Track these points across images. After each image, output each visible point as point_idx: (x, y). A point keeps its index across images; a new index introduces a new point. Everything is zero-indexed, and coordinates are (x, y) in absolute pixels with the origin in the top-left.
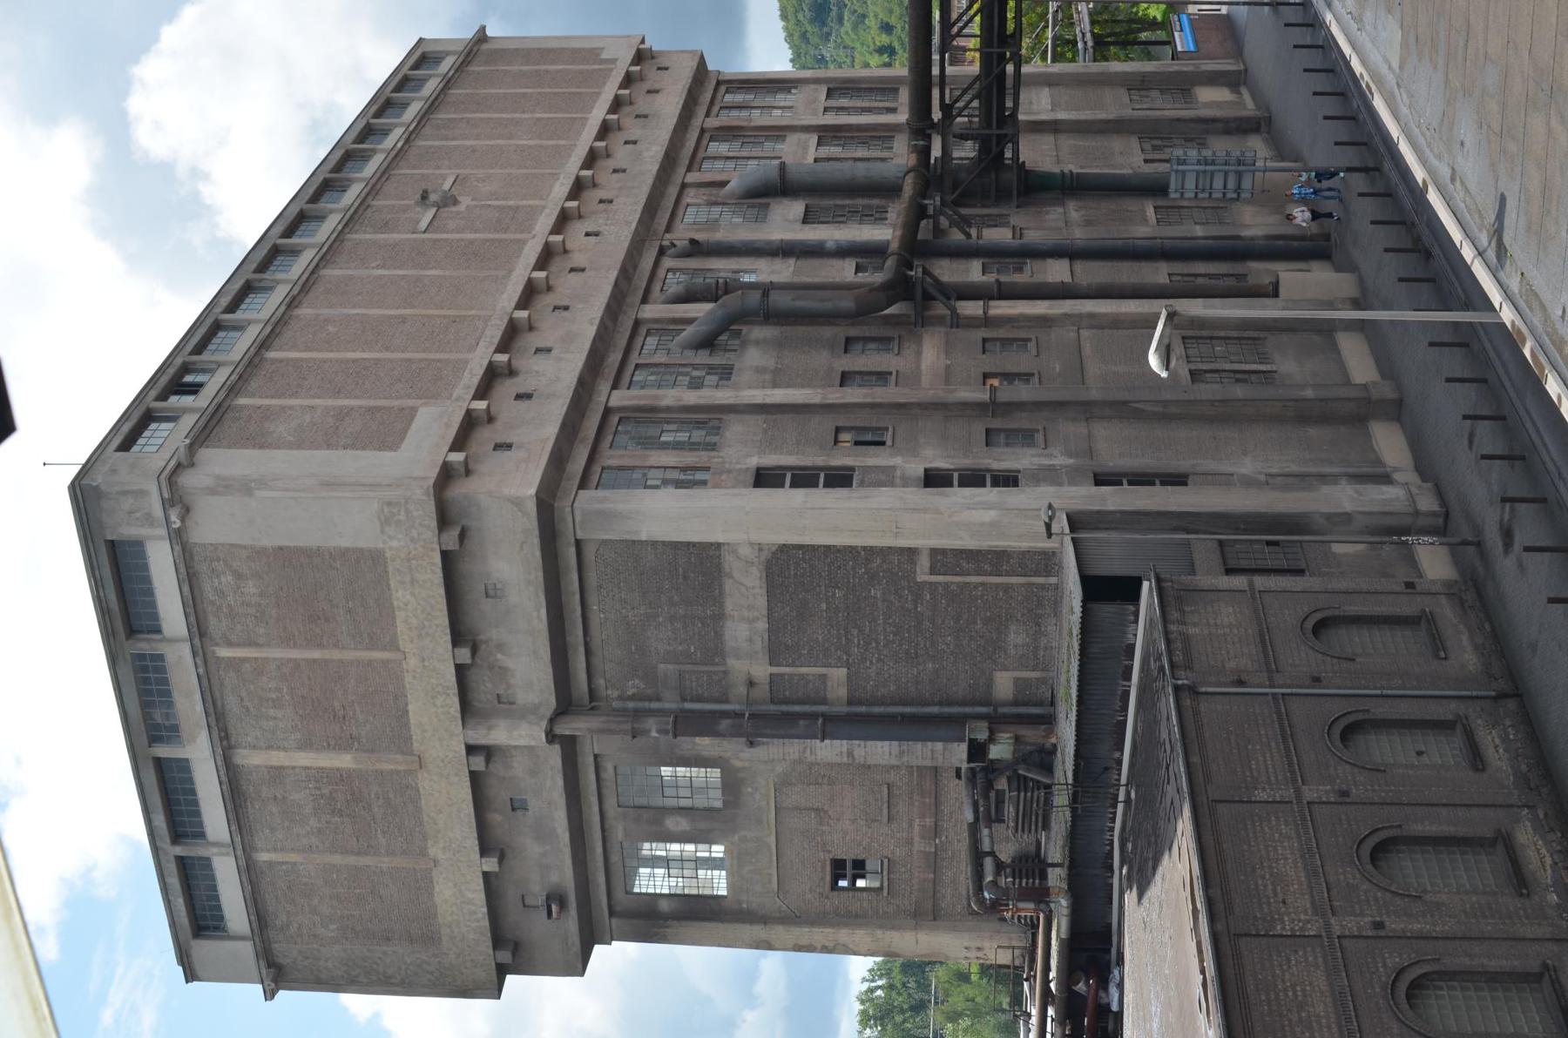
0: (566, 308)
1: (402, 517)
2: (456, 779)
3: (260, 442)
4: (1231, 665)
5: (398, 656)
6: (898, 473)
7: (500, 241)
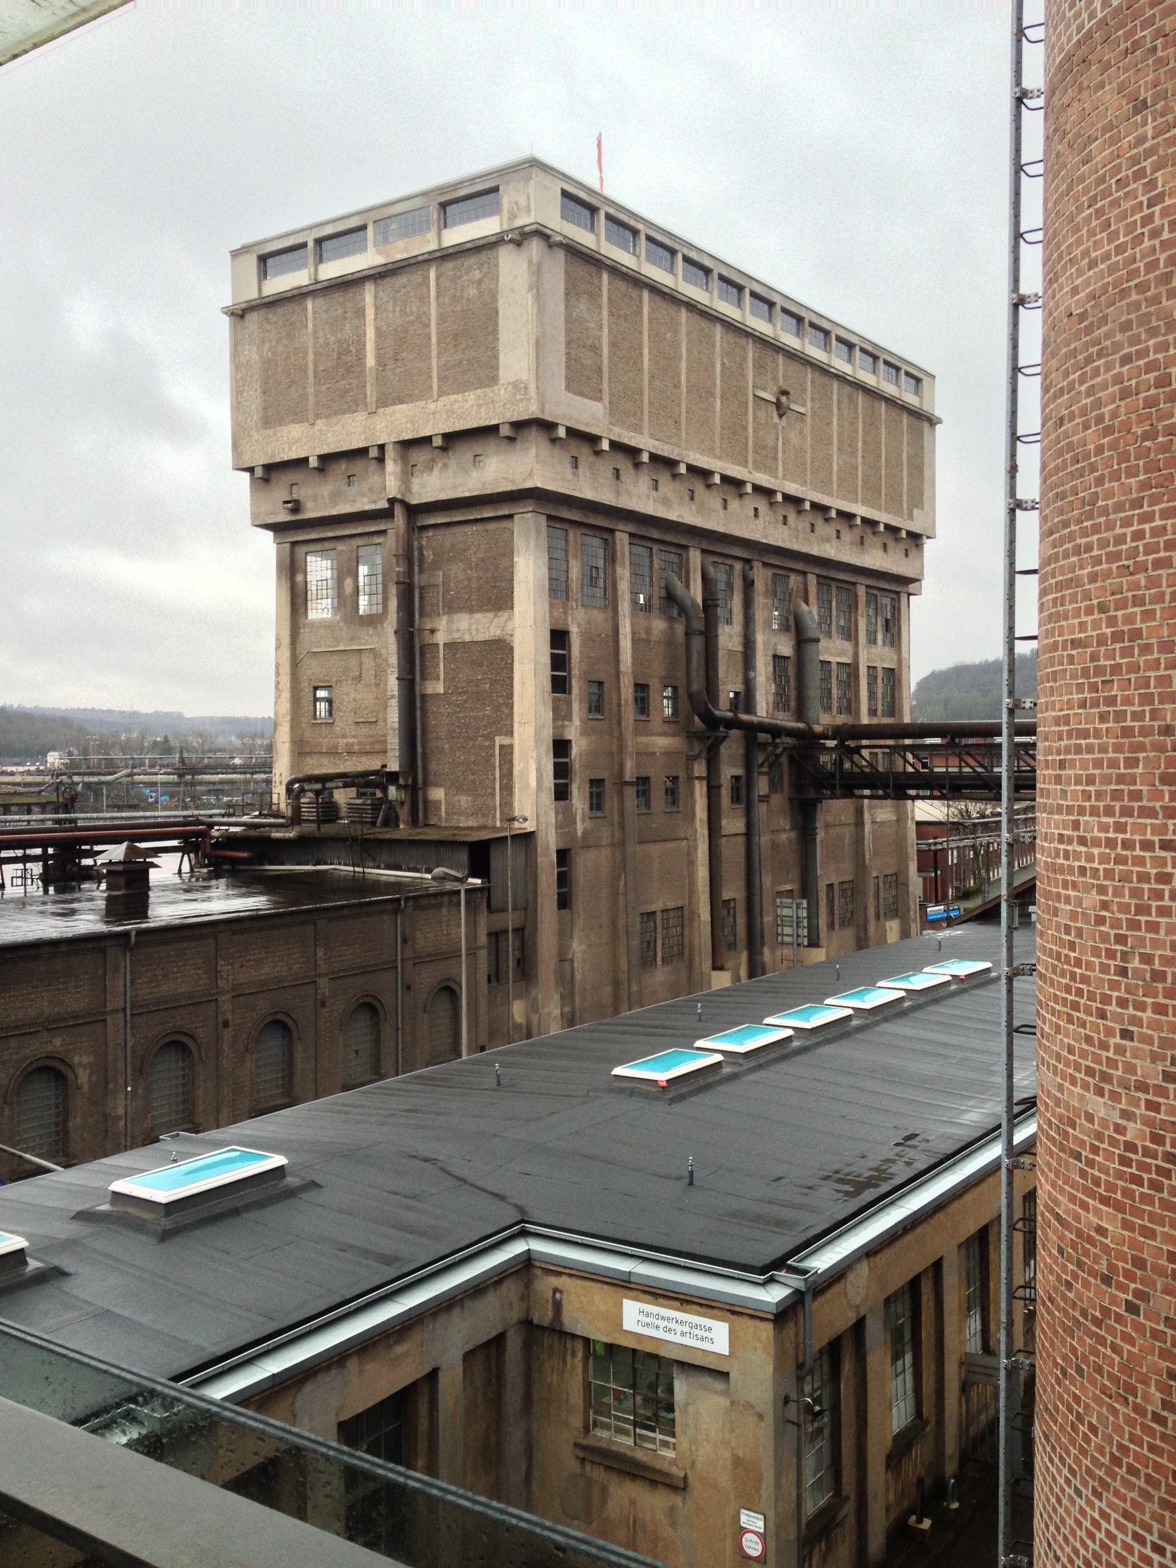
0: (692, 498)
1: (518, 397)
2: (363, 437)
3: (571, 292)
4: (418, 934)
5: (435, 397)
6: (567, 723)
7: (746, 449)
